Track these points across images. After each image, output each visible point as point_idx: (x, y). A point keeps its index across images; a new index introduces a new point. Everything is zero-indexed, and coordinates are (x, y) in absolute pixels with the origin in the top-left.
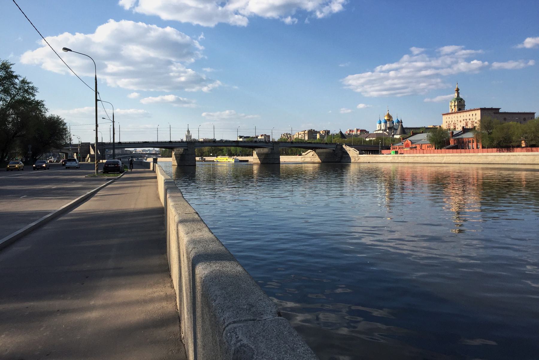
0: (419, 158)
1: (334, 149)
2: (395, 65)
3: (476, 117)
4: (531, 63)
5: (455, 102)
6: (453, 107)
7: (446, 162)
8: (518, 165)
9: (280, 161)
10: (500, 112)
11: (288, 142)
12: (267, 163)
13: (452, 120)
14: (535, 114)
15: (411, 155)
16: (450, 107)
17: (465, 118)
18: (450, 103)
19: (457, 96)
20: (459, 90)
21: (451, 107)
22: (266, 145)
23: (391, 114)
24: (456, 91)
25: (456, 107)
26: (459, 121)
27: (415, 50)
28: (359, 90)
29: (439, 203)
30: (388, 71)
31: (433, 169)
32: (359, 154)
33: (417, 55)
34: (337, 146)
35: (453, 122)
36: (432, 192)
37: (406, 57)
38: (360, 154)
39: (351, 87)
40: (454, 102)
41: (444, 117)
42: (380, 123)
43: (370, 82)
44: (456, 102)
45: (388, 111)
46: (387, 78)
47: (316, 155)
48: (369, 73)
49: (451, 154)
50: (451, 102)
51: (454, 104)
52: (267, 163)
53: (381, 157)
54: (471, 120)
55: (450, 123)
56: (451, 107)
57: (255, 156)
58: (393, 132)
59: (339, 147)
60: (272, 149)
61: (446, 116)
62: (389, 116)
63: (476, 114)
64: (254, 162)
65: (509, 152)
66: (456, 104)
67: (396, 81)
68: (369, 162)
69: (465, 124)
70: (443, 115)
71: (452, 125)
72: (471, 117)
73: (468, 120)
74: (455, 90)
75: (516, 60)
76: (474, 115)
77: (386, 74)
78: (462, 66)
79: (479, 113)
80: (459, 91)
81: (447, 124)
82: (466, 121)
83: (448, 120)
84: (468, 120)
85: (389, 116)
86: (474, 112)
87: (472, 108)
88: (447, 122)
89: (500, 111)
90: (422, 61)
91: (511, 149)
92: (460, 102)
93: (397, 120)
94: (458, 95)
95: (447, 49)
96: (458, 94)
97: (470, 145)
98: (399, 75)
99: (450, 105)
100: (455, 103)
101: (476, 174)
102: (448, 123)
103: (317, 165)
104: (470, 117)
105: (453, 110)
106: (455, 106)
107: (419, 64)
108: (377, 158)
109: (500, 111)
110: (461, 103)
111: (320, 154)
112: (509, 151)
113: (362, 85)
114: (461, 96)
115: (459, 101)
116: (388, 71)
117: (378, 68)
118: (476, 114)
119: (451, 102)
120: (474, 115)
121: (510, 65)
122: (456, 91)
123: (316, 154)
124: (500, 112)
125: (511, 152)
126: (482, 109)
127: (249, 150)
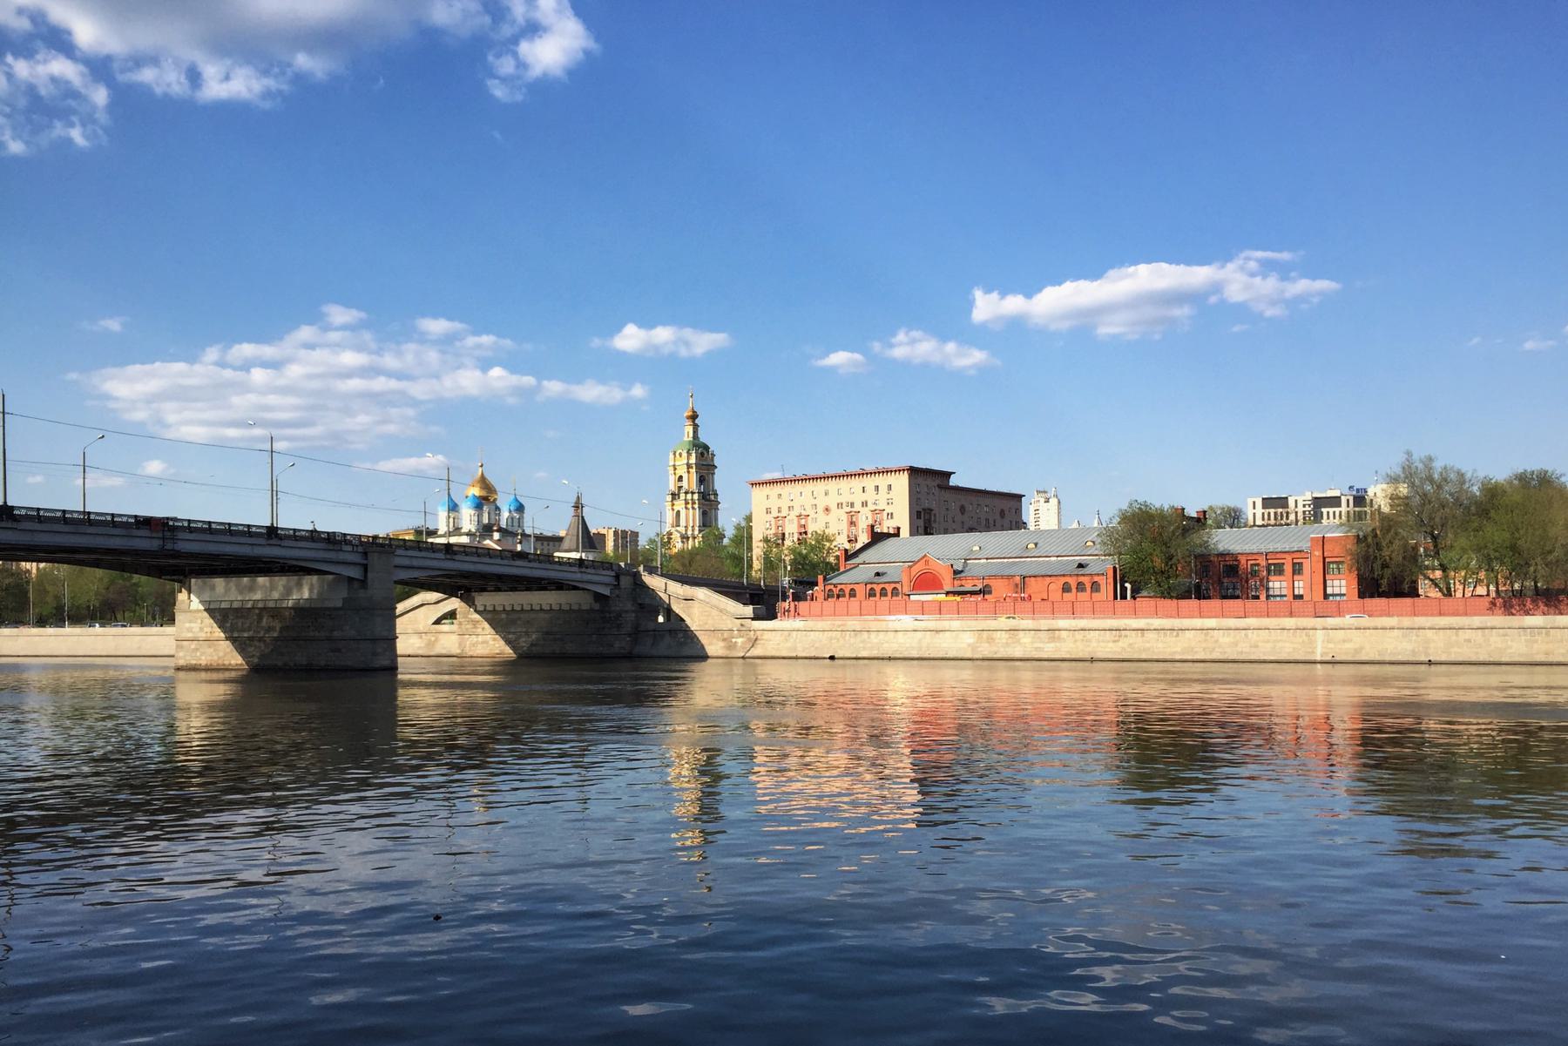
0: (1151, 635)
1: (606, 591)
2: (268, 351)
3: (889, 496)
4: (638, 391)
5: (689, 454)
6: (682, 471)
7: (1338, 658)
8: (1443, 666)
9: (400, 651)
10: (951, 484)
11: (433, 548)
12: (310, 671)
13: (791, 504)
14: (1023, 499)
15: (1416, 619)
16: (671, 470)
17: (844, 499)
18: (671, 456)
19: (691, 435)
20: (697, 416)
21: (675, 469)
22: (322, 555)
23: (491, 479)
24: (688, 418)
25: (693, 471)
26: (820, 509)
27: (339, 315)
28: (140, 415)
29: (1135, 833)
30: (246, 366)
31: (1105, 691)
32: (753, 619)
33: (344, 328)
34: (617, 577)
35: (796, 512)
36: (1139, 795)
37: (306, 333)
38: (756, 618)
39: (111, 405)
40: (688, 452)
41: (759, 494)
42: (453, 508)
43: (179, 394)
44: (694, 455)
45: (482, 466)
46: (244, 388)
47: (475, 623)
48: (180, 366)
49: (1232, 622)
50: (675, 454)
51: (686, 462)
52: (310, 671)
53: (900, 634)
54: (775, 514)
55: (783, 514)
56: (675, 469)
57: (196, 626)
58: (520, 543)
59: (626, 582)
60: (356, 585)
61: (767, 490)
62: (484, 483)
63: (890, 487)
64: (182, 662)
65: (1555, 614)
66: (693, 460)
67: (272, 399)
68: (832, 658)
69: (845, 518)
70: (752, 484)
71: (791, 521)
72: (870, 496)
73: (858, 507)
74: (686, 414)
75: (602, 381)
76: (883, 489)
77: (240, 375)
78: (468, 381)
79: (902, 482)
80: (697, 421)
81: (770, 517)
82: (849, 509)
83: (774, 504)
84: (858, 507)
85: (484, 483)
86: (882, 481)
87: (799, 475)
88: (768, 511)
89: (953, 481)
90: (359, 348)
91: (1559, 601)
92: (702, 454)
93: (517, 500)
94: (694, 432)
95: (436, 326)
96: (696, 427)
97: (1276, 585)
98: (281, 382)
99: (671, 463)
100: (688, 459)
101: (1323, 705)
102: (775, 514)
103: (244, 673)
104: (864, 497)
105: (680, 478)
106: (689, 466)
107: (350, 358)
108: (21, 641)
109: (953, 481)
110: (706, 460)
111: (504, 616)
112: (1556, 607)
113: (151, 399)
114: (703, 438)
115: (700, 451)
116: (246, 366)
117: (212, 354)
118: (890, 487)
119: (675, 454)
120: (883, 489)
121: (590, 392)
122: (688, 418)
123: (477, 616)
124: (951, 484)
125: (1562, 614)
126: (914, 471)
127: (145, 583)
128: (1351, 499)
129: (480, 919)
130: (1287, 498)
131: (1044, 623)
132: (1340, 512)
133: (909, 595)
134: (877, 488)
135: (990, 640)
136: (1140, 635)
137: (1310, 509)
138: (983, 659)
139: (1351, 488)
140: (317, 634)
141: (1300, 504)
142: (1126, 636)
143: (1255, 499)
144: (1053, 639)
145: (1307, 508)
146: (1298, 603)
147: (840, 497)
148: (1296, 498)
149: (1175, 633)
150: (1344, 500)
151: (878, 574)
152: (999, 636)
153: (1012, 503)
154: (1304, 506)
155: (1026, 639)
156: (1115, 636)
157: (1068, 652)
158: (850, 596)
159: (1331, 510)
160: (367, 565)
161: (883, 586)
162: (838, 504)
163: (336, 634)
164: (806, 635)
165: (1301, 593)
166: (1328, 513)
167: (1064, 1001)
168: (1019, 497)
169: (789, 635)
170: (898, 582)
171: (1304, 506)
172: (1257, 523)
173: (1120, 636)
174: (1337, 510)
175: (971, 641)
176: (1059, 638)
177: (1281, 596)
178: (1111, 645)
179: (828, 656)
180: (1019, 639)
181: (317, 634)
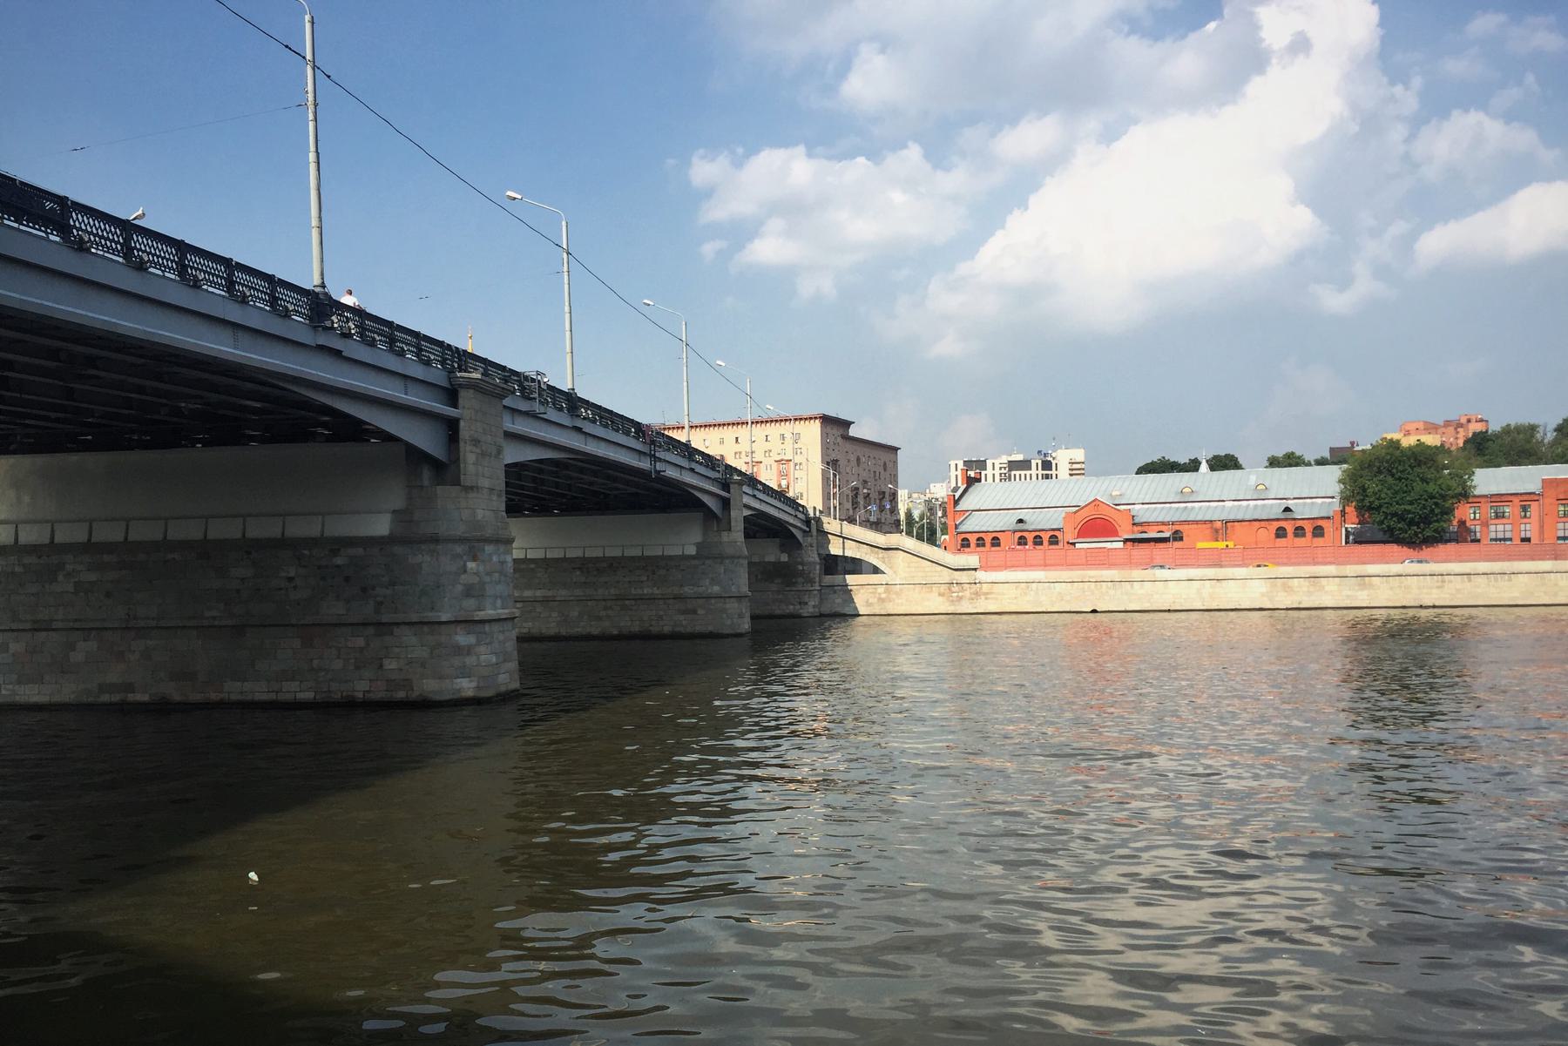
104: (768, 446)
120: (789, 440)
124: (851, 434)
128: (1040, 462)
129: (718, 960)
130: (985, 461)
131: (1351, 570)
132: (1031, 475)
133: (1074, 544)
134: (783, 437)
135: (1288, 590)
136: (1466, 580)
137: (1005, 472)
138: (1287, 609)
139: (1039, 452)
140: (656, 591)
141: (997, 467)
142: (1450, 582)
143: (957, 462)
144: (1363, 587)
145: (1003, 471)
146: (1526, 546)
147: (737, 445)
148: (993, 461)
149: (1506, 577)
150: (1034, 463)
151: (1021, 521)
152: (1296, 584)
153: (885, 456)
154: (1001, 468)
155: (1331, 586)
156: (1438, 581)
157: (1415, 600)
158: (1036, 543)
159: (1023, 473)
160: (729, 499)
161: (1052, 533)
162: (736, 453)
163: (688, 590)
164: (1049, 588)
165: (1528, 536)
166: (1015, 475)
167: (1261, 975)
168: (896, 449)
169: (1028, 587)
170: (1059, 530)
171: (1001, 468)
172: (320, 517)
173: (1443, 581)
174: (1028, 473)
175: (1264, 590)
176: (1371, 585)
177: (1505, 540)
178: (1434, 591)
179: (1090, 610)
180: (1323, 587)
181: (656, 591)
